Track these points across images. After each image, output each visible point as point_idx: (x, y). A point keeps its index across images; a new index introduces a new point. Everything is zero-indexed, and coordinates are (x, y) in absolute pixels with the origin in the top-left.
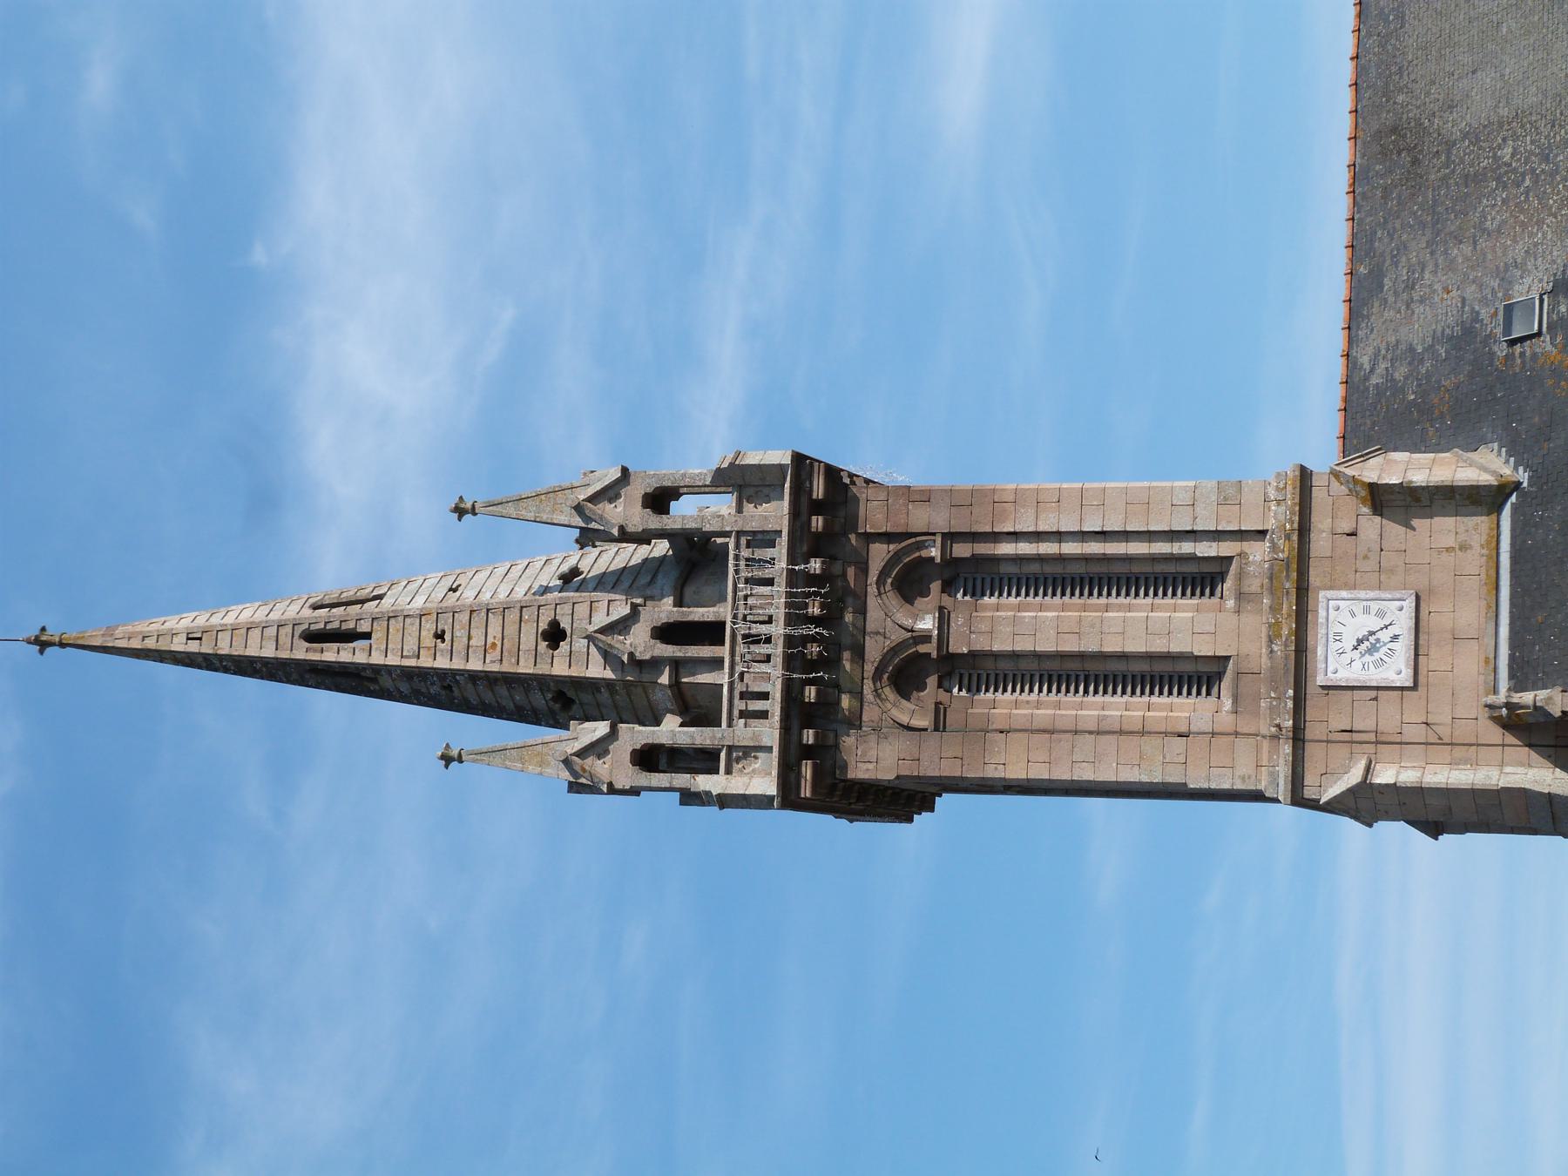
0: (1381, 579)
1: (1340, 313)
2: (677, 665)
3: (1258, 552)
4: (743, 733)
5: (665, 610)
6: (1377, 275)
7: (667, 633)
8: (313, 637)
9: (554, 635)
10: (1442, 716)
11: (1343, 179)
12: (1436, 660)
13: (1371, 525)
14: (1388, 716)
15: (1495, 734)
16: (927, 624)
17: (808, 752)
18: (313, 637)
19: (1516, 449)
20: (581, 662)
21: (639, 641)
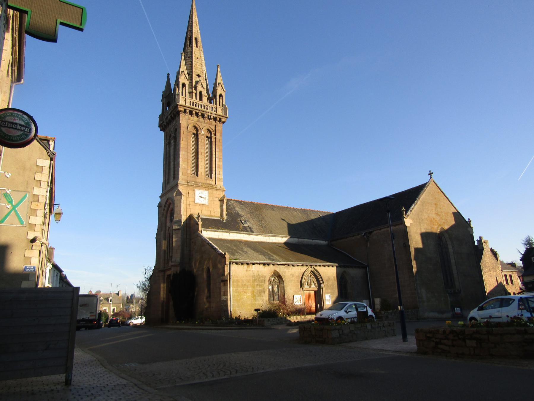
0: (210, 200)
1: (240, 200)
2: (196, 94)
3: (213, 183)
4: (188, 101)
5: (204, 93)
6: (242, 204)
7: (201, 93)
8: (196, 39)
9: (199, 76)
10: (191, 207)
11: (253, 201)
12: (199, 207)
13: (217, 199)
14: (191, 199)
15: (188, 215)
16: (203, 133)
17: (185, 110)
18: (196, 39)
19: (227, 220)
20: (195, 78)
21: (199, 88)
